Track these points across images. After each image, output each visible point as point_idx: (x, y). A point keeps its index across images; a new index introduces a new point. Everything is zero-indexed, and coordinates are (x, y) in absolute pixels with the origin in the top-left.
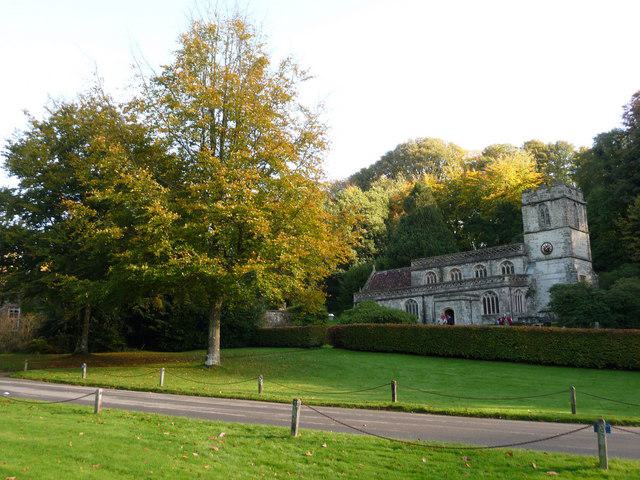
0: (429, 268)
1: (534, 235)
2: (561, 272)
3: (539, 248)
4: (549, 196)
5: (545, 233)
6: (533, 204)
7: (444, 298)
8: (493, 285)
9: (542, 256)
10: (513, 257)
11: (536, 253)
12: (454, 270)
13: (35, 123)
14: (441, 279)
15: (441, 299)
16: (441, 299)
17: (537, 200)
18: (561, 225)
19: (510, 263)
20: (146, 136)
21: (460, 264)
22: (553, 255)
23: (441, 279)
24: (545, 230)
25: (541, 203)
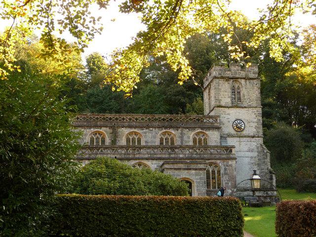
0: (96, 126)
1: (226, 109)
2: (252, 151)
3: (231, 123)
4: (243, 74)
5: (238, 109)
6: (228, 79)
7: (182, 166)
8: (218, 156)
9: (233, 132)
10: (209, 128)
11: (228, 129)
12: (131, 134)
13: (106, 8)
14: (114, 142)
15: (176, 166)
16: (176, 166)
17: (231, 76)
18: (255, 105)
19: (204, 134)
20: (294, 65)
21: (142, 128)
22: (244, 133)
23: (114, 142)
24: (237, 107)
25: (235, 79)
